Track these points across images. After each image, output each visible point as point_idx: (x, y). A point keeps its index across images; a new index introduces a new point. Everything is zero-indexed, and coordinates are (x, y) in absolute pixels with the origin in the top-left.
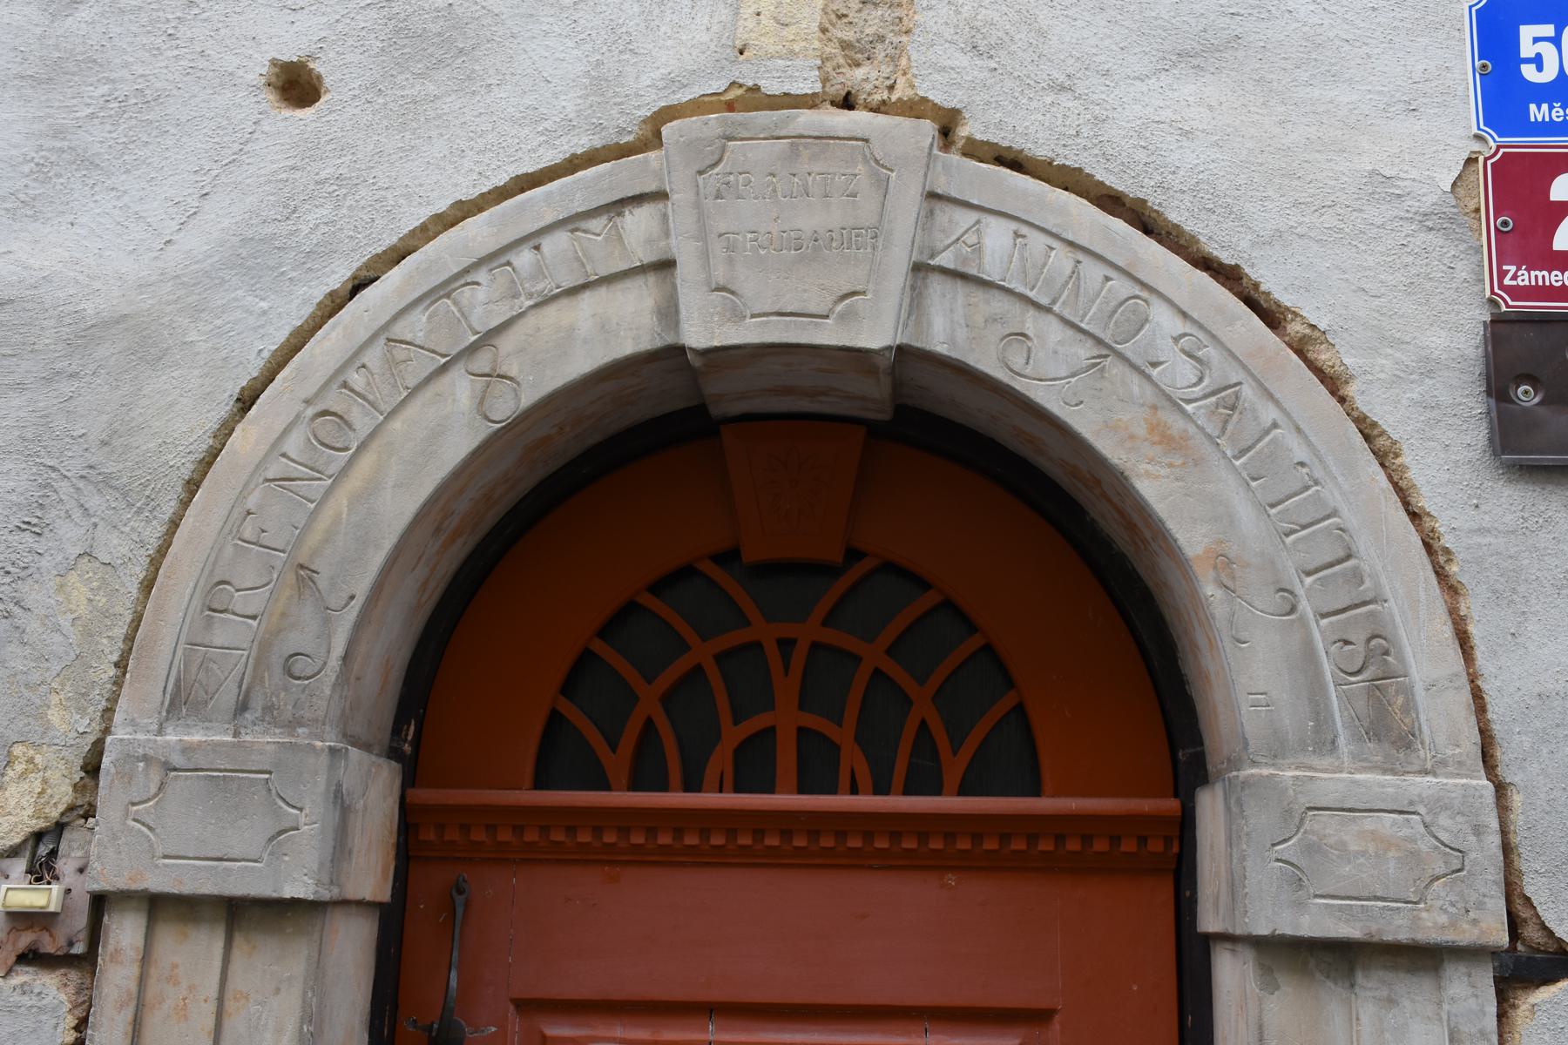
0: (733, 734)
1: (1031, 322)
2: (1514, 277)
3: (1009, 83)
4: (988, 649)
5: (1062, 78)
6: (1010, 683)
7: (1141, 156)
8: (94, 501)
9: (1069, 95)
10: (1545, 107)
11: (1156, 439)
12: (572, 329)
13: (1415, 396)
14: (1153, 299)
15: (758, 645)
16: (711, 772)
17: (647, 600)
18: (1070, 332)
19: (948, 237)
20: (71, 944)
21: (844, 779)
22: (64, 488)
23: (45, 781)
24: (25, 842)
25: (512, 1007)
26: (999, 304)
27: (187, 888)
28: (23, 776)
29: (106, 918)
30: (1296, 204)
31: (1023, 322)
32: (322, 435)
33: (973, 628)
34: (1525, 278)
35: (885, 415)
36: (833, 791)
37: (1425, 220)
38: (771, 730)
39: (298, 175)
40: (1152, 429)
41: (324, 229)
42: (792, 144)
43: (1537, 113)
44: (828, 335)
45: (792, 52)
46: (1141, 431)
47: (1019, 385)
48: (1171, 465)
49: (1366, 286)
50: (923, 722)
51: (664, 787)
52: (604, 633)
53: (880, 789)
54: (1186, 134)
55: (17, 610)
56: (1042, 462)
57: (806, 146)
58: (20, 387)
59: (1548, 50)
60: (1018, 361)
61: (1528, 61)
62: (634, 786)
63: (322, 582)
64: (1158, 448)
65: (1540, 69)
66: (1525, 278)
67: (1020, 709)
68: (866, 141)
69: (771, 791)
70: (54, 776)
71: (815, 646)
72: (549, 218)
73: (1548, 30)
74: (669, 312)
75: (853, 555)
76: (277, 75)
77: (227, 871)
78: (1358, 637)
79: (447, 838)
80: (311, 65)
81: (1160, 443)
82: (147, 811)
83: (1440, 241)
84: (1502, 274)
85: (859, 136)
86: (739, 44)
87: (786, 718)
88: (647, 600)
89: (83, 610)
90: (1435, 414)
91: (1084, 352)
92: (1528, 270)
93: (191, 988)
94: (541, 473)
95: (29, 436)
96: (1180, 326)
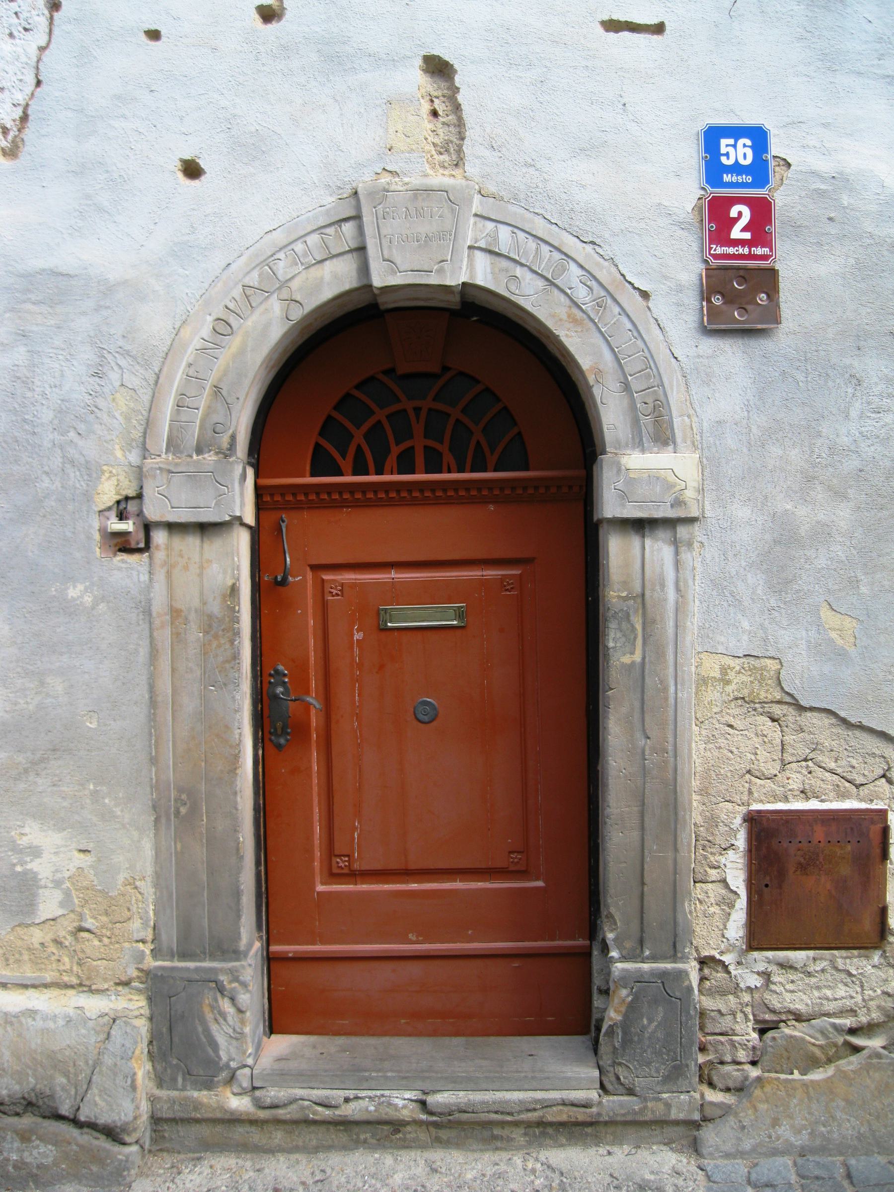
0: (395, 450)
1: (519, 271)
2: (715, 250)
3: (507, 163)
4: (505, 408)
5: (530, 161)
6: (516, 424)
7: (564, 196)
8: (123, 362)
9: (533, 168)
10: (730, 175)
11: (571, 320)
12: (322, 278)
13: (674, 301)
14: (569, 261)
15: (405, 410)
16: (387, 467)
17: (356, 393)
18: (534, 276)
19: (482, 234)
20: (138, 544)
21: (445, 467)
22: (109, 357)
23: (118, 480)
24: (113, 505)
25: (308, 569)
26: (505, 263)
27: (183, 519)
28: (109, 478)
29: (152, 534)
30: (629, 218)
31: (515, 271)
32: (217, 329)
33: (498, 400)
34: (720, 250)
35: (458, 307)
36: (441, 472)
37: (682, 225)
38: (412, 448)
39: (195, 213)
40: (569, 316)
41: (210, 237)
42: (414, 194)
43: (727, 178)
44: (433, 280)
45: (412, 149)
46: (565, 317)
47: (513, 298)
48: (576, 332)
49: (656, 254)
50: (478, 442)
51: (367, 473)
52: (335, 408)
53: (461, 470)
54: (583, 186)
55: (96, 410)
56: (529, 328)
57: (421, 195)
58: (84, 313)
59: (731, 150)
60: (513, 288)
61: (724, 155)
62: (355, 473)
63: (224, 393)
64: (571, 325)
65: (728, 158)
66: (720, 250)
67: (519, 434)
68: (447, 192)
69: (414, 473)
70: (122, 478)
71: (430, 410)
72: (309, 230)
73: (732, 141)
74: (364, 269)
75: (446, 369)
76: (182, 166)
77: (200, 511)
78: (650, 400)
79: (275, 499)
80: (197, 161)
81: (572, 322)
82: (163, 489)
83: (686, 234)
84: (710, 249)
85: (443, 189)
86: (388, 146)
87: (419, 443)
88: (356, 393)
89: (124, 409)
90: (682, 308)
91: (540, 283)
92: (721, 247)
93: (189, 559)
94: (306, 337)
95: (92, 335)
96: (580, 272)
